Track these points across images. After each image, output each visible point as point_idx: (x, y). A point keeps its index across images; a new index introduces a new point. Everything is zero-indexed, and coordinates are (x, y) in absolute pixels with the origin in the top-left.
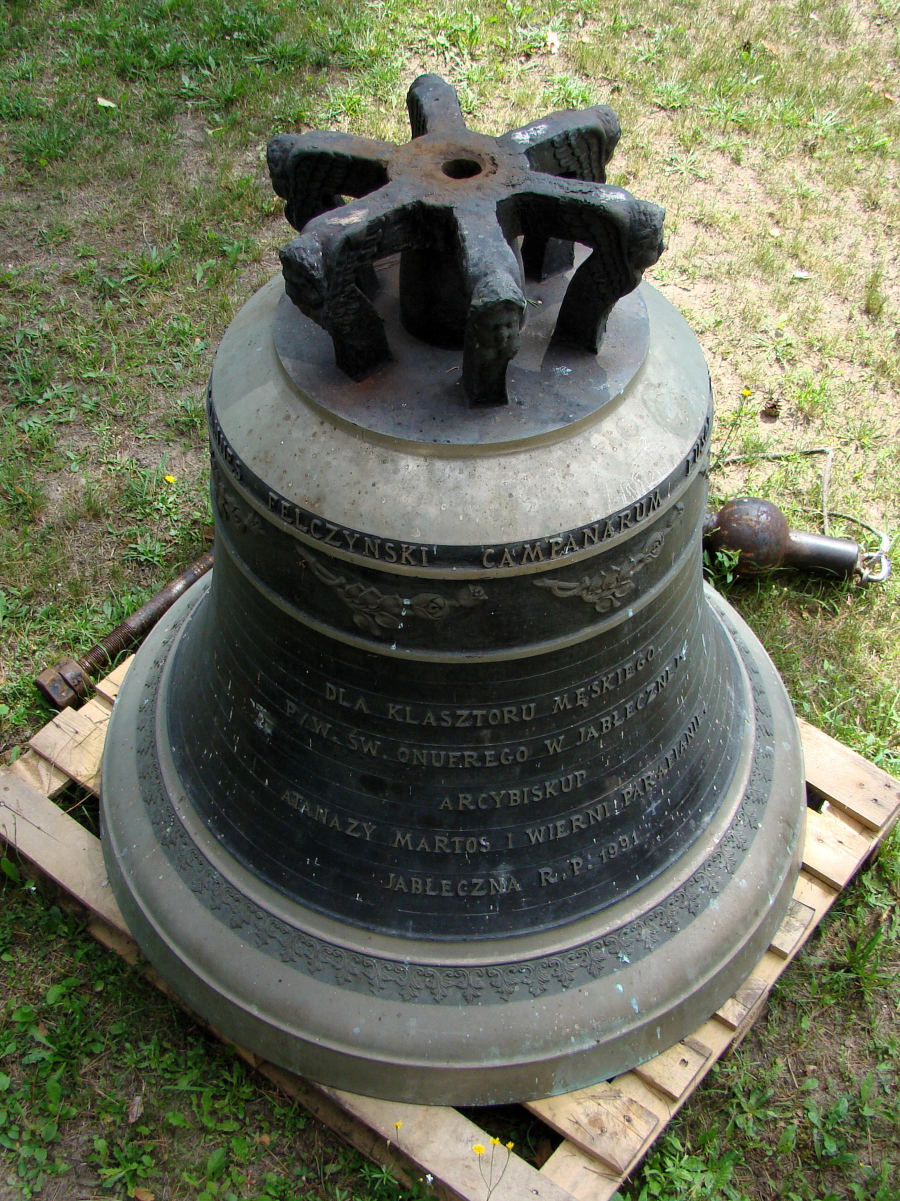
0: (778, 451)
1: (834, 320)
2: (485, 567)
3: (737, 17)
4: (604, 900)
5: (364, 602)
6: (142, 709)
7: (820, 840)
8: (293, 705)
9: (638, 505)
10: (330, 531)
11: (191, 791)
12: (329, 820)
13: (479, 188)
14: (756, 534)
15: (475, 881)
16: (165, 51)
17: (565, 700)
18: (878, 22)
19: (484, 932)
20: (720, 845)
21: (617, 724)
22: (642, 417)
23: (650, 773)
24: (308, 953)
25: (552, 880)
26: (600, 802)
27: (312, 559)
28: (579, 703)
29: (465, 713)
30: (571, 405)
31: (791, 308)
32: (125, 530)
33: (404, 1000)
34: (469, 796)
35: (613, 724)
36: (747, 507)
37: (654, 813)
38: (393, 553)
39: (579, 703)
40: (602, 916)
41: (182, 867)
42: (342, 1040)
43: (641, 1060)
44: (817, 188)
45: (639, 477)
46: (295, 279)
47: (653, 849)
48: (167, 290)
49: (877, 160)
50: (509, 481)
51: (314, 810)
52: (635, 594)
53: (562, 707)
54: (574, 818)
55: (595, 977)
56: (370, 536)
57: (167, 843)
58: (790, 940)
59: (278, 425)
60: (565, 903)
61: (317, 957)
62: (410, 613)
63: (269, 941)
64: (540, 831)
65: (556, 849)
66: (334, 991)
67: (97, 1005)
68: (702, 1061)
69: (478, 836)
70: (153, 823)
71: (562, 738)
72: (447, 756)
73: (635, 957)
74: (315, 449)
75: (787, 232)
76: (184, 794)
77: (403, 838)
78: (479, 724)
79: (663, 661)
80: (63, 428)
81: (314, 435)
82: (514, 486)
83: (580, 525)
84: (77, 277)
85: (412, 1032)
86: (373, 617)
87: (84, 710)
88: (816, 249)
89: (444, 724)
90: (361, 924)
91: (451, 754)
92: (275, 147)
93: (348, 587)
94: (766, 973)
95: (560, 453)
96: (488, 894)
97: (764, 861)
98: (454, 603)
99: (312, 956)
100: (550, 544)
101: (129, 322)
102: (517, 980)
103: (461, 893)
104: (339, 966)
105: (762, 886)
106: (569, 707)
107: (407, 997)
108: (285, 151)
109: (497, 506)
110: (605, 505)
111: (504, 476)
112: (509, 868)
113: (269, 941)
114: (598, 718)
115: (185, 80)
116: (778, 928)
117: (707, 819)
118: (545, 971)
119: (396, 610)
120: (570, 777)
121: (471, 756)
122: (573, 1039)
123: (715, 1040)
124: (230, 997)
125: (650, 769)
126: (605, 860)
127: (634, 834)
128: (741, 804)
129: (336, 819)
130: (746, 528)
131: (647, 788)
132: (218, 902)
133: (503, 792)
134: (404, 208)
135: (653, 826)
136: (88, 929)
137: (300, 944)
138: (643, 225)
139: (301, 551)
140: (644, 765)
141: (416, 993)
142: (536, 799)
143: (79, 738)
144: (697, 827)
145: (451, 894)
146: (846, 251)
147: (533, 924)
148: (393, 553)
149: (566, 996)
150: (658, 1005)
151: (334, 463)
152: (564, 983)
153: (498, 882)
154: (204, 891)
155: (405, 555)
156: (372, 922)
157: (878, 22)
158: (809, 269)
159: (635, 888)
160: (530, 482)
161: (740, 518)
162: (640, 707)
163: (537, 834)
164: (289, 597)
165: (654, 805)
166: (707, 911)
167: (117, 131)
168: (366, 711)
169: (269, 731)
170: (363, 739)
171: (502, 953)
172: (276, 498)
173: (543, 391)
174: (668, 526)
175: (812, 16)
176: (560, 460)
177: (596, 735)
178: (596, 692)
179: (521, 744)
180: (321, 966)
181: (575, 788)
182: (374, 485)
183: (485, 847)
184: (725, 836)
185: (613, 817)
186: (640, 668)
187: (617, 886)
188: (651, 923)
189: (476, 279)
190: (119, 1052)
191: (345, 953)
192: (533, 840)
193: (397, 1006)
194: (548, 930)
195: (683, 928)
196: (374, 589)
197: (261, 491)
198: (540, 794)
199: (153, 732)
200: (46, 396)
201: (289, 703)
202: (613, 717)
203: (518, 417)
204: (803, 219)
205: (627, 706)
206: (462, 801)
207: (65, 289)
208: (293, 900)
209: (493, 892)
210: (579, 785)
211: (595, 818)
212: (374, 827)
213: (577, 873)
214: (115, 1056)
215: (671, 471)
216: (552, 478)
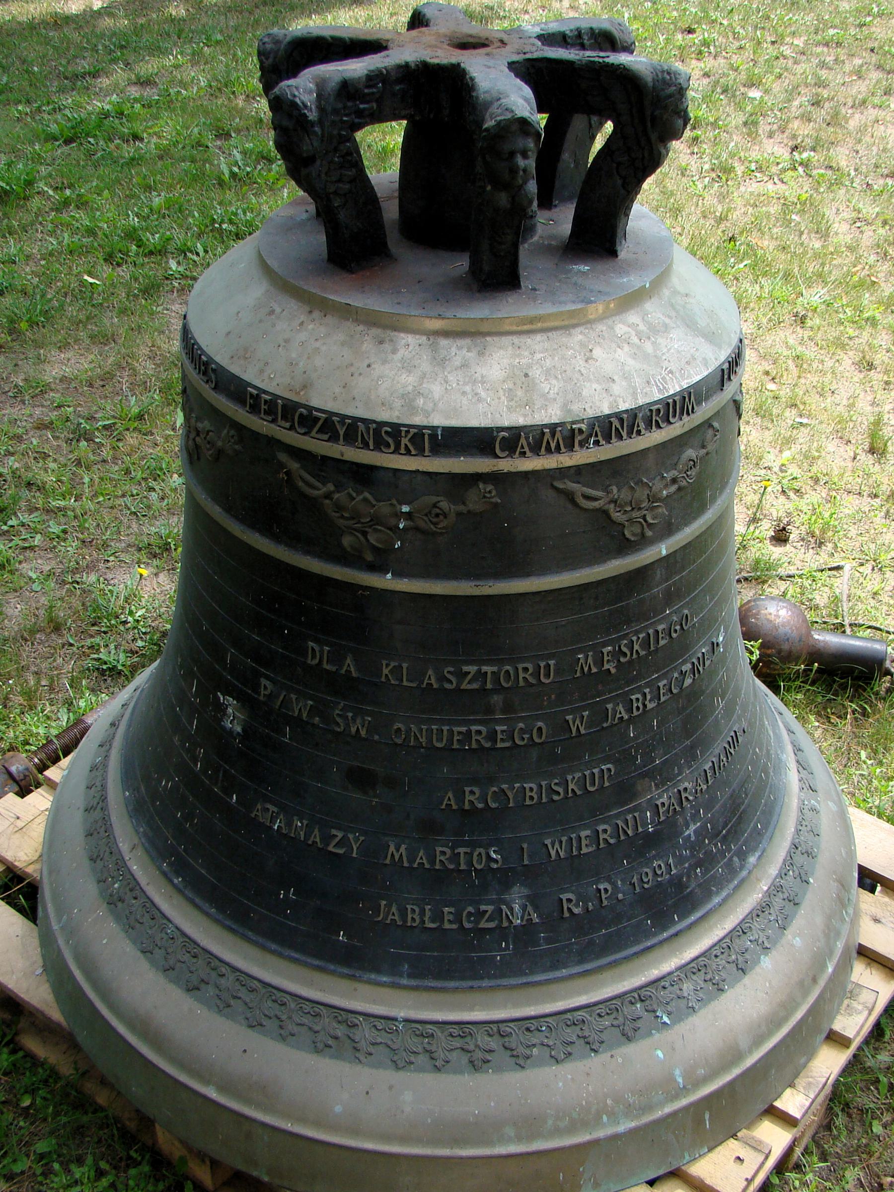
0: (792, 570)
1: (836, 458)
2: (497, 457)
3: (721, 219)
4: (637, 942)
5: (356, 516)
6: (94, 768)
7: (877, 920)
8: (268, 683)
9: (671, 401)
10: (317, 419)
11: (145, 834)
12: (307, 835)
13: (487, 54)
14: (776, 628)
15: (483, 908)
16: (153, 240)
17: (590, 660)
18: (858, 224)
19: (495, 977)
20: (768, 894)
21: (650, 706)
22: (670, 317)
23: (686, 784)
24: (279, 1014)
25: (576, 911)
26: (630, 811)
27: (294, 465)
28: (606, 666)
29: (472, 669)
30: (592, 291)
31: (793, 449)
32: (89, 642)
33: (398, 1068)
34: (476, 790)
35: (645, 706)
36: (766, 602)
37: (693, 838)
38: (390, 440)
39: (606, 666)
40: (637, 962)
41: (130, 925)
42: (318, 1124)
43: (687, 1158)
44: (810, 352)
45: (671, 372)
46: (286, 123)
47: (693, 885)
48: (144, 434)
49: (868, 329)
50: (523, 361)
51: (289, 824)
52: (669, 529)
53: (586, 669)
54: (601, 828)
55: (629, 1039)
56: (363, 420)
57: (113, 901)
58: (854, 1023)
59: (260, 321)
60: (591, 943)
61: (290, 1018)
62: (409, 523)
63: (232, 1002)
64: (561, 842)
65: (577, 868)
66: (311, 1060)
67: (22, 1124)
68: (761, 1158)
69: (487, 846)
70: (99, 882)
71: (586, 713)
72: (451, 732)
73: (678, 1017)
74: (303, 336)
75: (784, 387)
76: (136, 841)
77: (397, 851)
78: (489, 686)
79: (698, 641)
80: (28, 553)
81: (302, 324)
82: (530, 366)
83: (607, 411)
84: (52, 423)
85: (408, 1109)
86: (365, 534)
87: (30, 798)
88: (813, 400)
89: (447, 686)
90: (346, 971)
91: (456, 729)
92: (266, 40)
93: (336, 496)
94: (828, 1064)
95: (580, 337)
96: (499, 927)
97: (819, 920)
98: (462, 508)
99: (284, 1017)
100: (573, 430)
101: (104, 461)
102: (535, 1041)
103: (467, 925)
104: (317, 1028)
105: (818, 948)
106: (594, 670)
107: (401, 1064)
108: (277, 42)
109: (511, 386)
110: (634, 394)
111: (519, 356)
112: (525, 891)
113: (232, 1002)
114: (628, 693)
115: (173, 265)
116: (838, 1012)
117: (752, 860)
118: (569, 1030)
119: (393, 521)
120: (596, 771)
121: (479, 732)
122: (605, 1118)
123: (775, 1138)
124: (183, 1078)
125: (686, 779)
126: (638, 890)
127: (671, 861)
128: (789, 852)
129: (316, 832)
130: (765, 622)
131: (685, 803)
132: (172, 962)
133: (517, 785)
134: (407, 65)
135: (692, 855)
136: (17, 1038)
137: (270, 1003)
138: (666, 84)
139: (283, 457)
140: (680, 774)
141: (412, 1059)
142: (556, 798)
143: (20, 824)
144: (742, 867)
145: (454, 926)
146: (845, 402)
147: (554, 967)
148: (390, 440)
149: (595, 1062)
150: (706, 1080)
151: (324, 348)
152: (593, 1047)
153: (511, 909)
154: (157, 950)
155: (405, 441)
156: (360, 969)
157: (858, 224)
158: (809, 417)
159: (672, 931)
160: (548, 363)
161: (758, 613)
162: (675, 691)
163: (557, 845)
164: (266, 531)
165: (693, 828)
166: (758, 969)
167: (101, 304)
168: (354, 675)
169: (239, 729)
170: (350, 715)
171: (516, 1005)
172: (255, 392)
173: (560, 281)
174: (703, 447)
175: (794, 217)
176: (582, 345)
177: (626, 717)
178: (625, 655)
179: (538, 718)
180: (296, 1029)
181: (602, 787)
182: (369, 366)
183: (496, 861)
184: (773, 884)
185: (646, 834)
186: (674, 635)
187: (653, 926)
188: (694, 977)
189: (487, 105)
190: (45, 1174)
191: (324, 1011)
192: (553, 853)
193: (388, 1076)
194: (571, 977)
195: (732, 986)
196: (367, 495)
197: (237, 390)
198: (561, 790)
199: (104, 787)
200: (10, 523)
201: (264, 681)
202: (645, 695)
203: (535, 299)
204: (799, 377)
205: (661, 684)
206: (468, 797)
207: (38, 433)
208: (263, 948)
209: (505, 924)
210: (607, 784)
211: (625, 832)
212: (362, 838)
213: (605, 903)
214: (40, 1179)
215: (706, 374)
216: (573, 361)
